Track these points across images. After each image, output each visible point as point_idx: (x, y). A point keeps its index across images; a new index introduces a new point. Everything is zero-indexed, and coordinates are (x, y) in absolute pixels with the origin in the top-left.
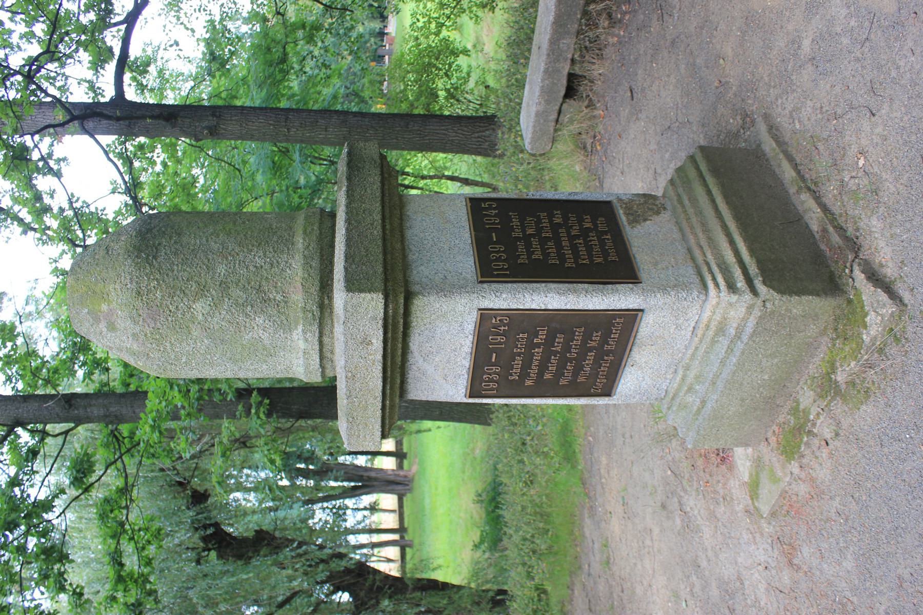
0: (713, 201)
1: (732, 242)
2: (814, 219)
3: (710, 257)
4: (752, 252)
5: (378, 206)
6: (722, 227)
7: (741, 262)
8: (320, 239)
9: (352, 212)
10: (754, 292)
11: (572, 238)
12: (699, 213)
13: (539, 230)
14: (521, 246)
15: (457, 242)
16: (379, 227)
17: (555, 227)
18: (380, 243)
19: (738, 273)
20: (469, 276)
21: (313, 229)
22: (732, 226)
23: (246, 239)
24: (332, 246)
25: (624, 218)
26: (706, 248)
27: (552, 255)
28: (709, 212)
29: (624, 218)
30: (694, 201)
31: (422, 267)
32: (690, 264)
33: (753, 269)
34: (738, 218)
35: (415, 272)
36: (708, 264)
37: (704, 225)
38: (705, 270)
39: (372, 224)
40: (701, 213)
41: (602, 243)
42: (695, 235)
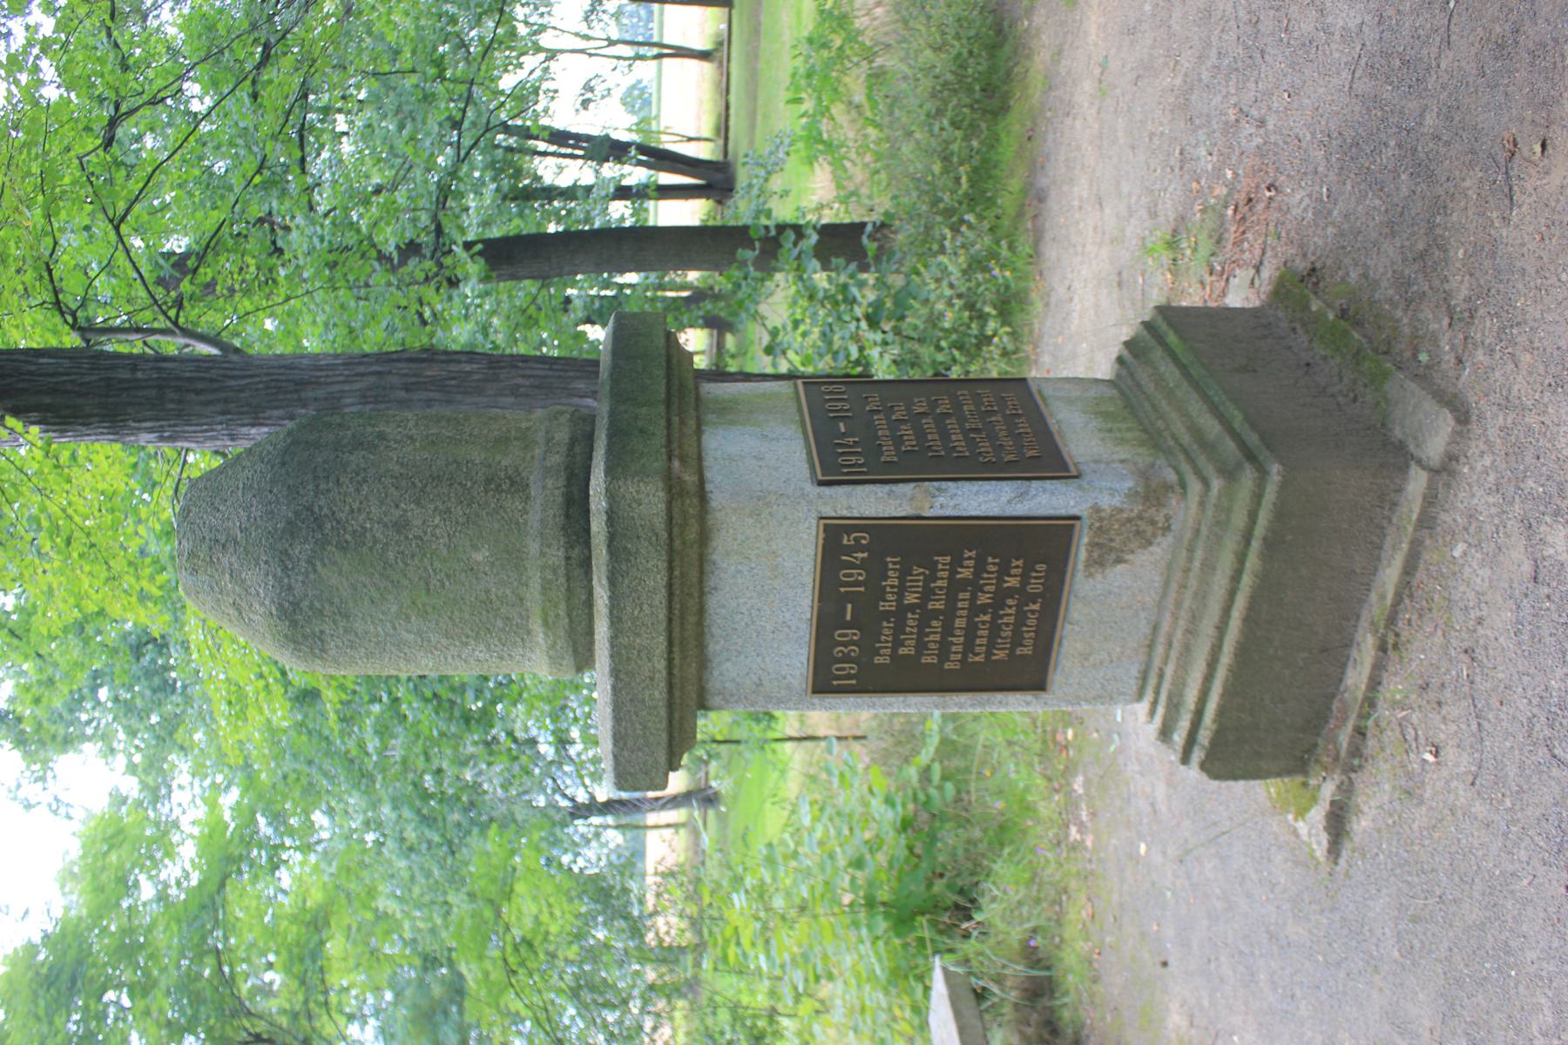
0: (1232, 593)
1: (1208, 679)
2: (1356, 678)
3: (1169, 671)
4: (1221, 712)
5: (661, 642)
6: (1213, 646)
7: (1199, 713)
8: (571, 631)
9: (619, 654)
10: (1185, 759)
11: (975, 610)
12: (1201, 596)
13: (927, 594)
14: (887, 628)
15: (788, 615)
16: (663, 684)
17: (955, 586)
18: (663, 712)
19: (1184, 724)
20: (795, 683)
21: (557, 616)
22: (1226, 659)
23: (454, 624)
24: (590, 632)
25: (1083, 555)
26: (1174, 654)
27: (932, 646)
28: (1208, 627)
29: (1083, 555)
30: (1209, 567)
31: (728, 664)
32: (1142, 658)
33: (1204, 736)
34: (1242, 651)
35: (716, 673)
36: (1161, 676)
37: (1195, 618)
38: (1152, 681)
39: (652, 679)
40: (1204, 597)
41: (1021, 617)
42: (1175, 618)
